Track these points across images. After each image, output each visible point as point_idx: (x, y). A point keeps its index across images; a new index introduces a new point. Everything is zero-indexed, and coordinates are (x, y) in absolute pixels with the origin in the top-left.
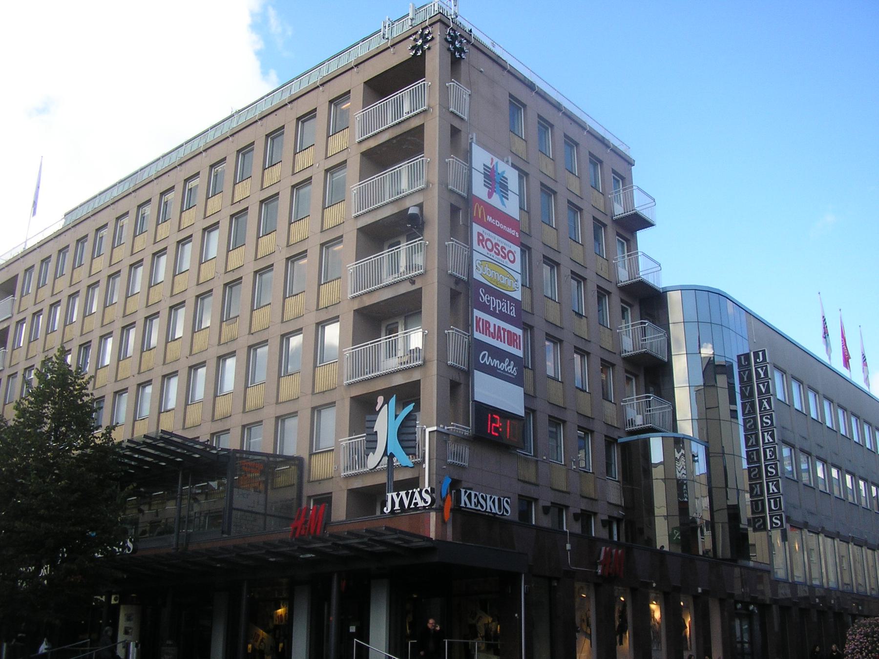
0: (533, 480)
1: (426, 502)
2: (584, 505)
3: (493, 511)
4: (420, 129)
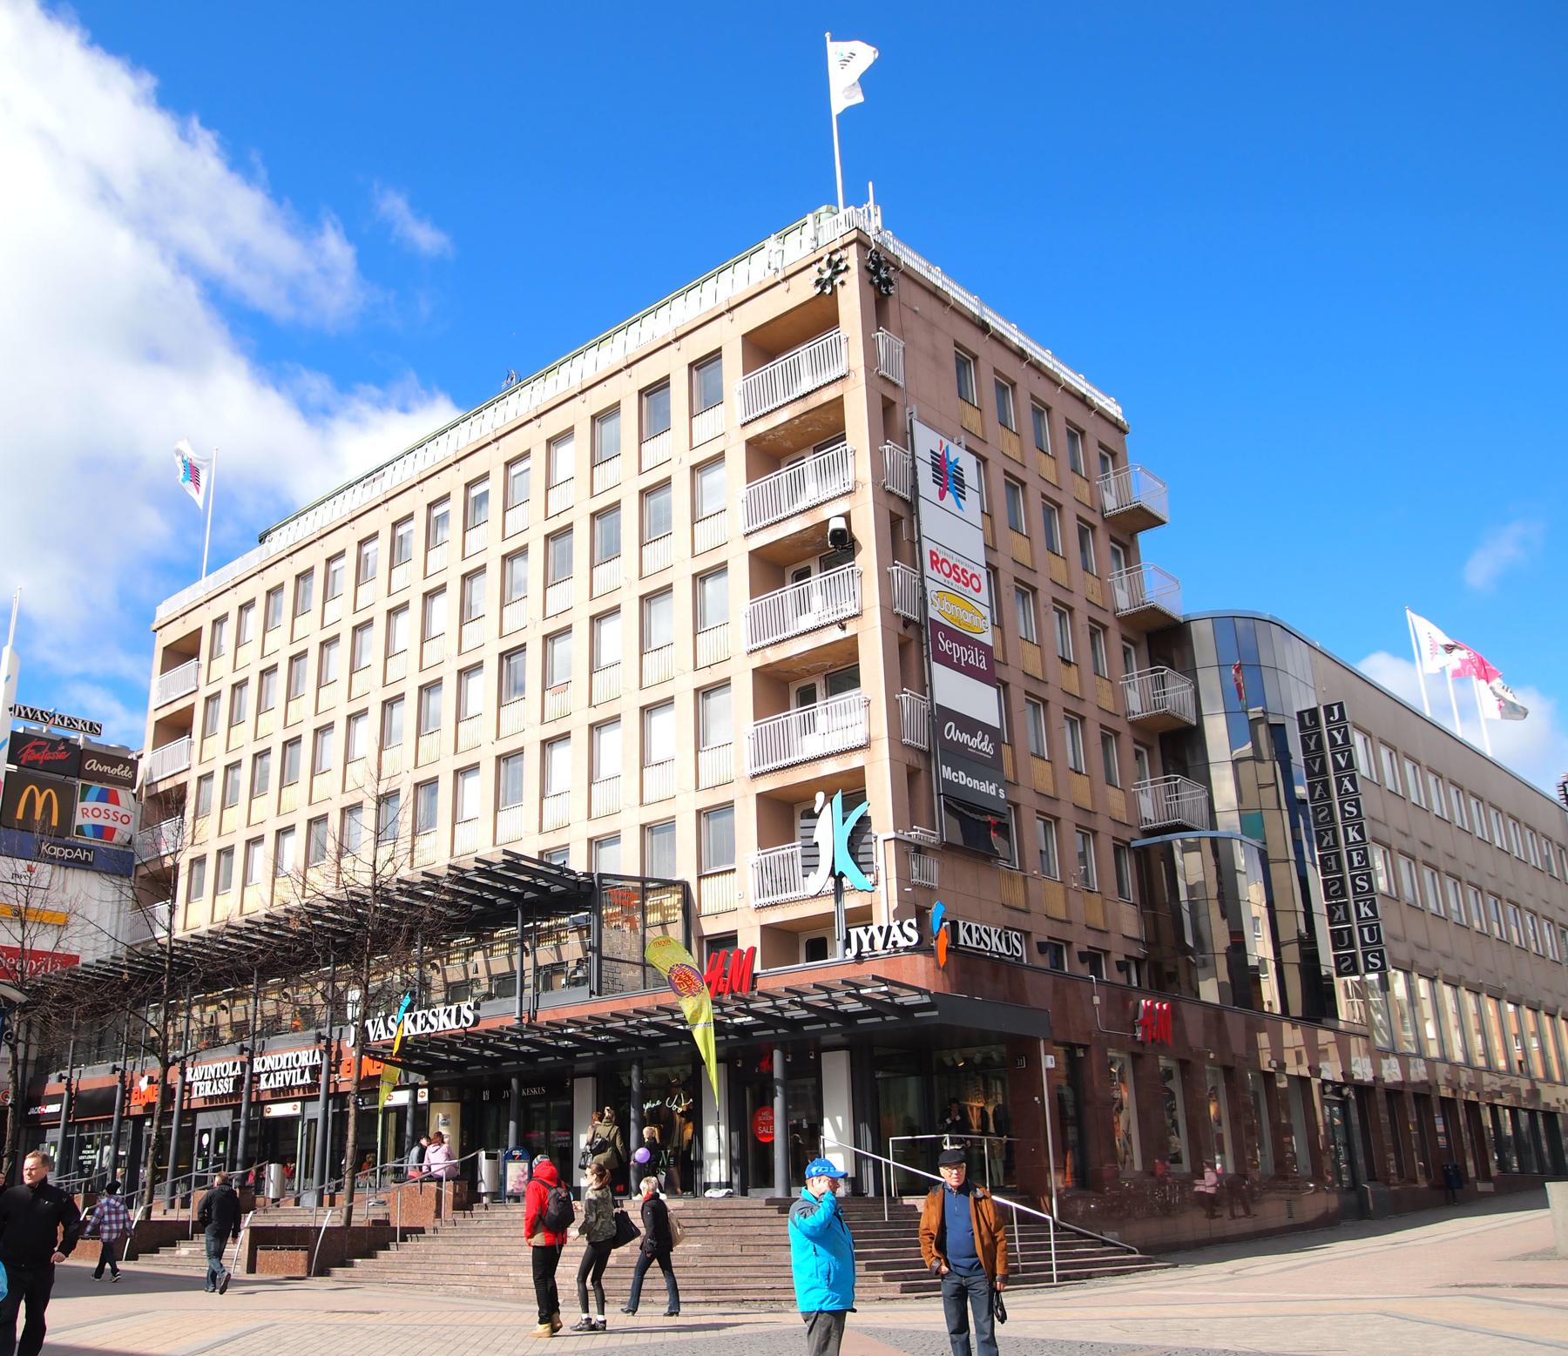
0: (1022, 905)
1: (910, 939)
2: (1091, 940)
3: (1001, 951)
4: (838, 403)
